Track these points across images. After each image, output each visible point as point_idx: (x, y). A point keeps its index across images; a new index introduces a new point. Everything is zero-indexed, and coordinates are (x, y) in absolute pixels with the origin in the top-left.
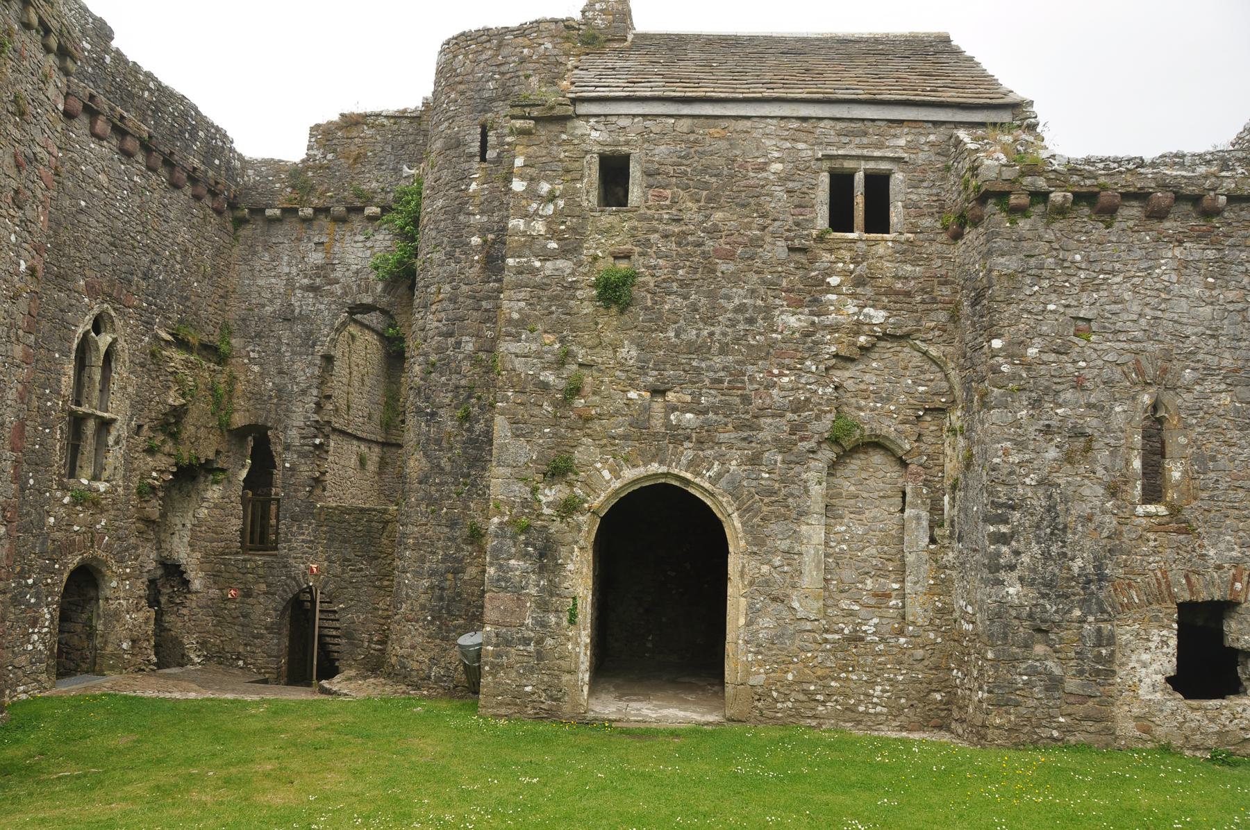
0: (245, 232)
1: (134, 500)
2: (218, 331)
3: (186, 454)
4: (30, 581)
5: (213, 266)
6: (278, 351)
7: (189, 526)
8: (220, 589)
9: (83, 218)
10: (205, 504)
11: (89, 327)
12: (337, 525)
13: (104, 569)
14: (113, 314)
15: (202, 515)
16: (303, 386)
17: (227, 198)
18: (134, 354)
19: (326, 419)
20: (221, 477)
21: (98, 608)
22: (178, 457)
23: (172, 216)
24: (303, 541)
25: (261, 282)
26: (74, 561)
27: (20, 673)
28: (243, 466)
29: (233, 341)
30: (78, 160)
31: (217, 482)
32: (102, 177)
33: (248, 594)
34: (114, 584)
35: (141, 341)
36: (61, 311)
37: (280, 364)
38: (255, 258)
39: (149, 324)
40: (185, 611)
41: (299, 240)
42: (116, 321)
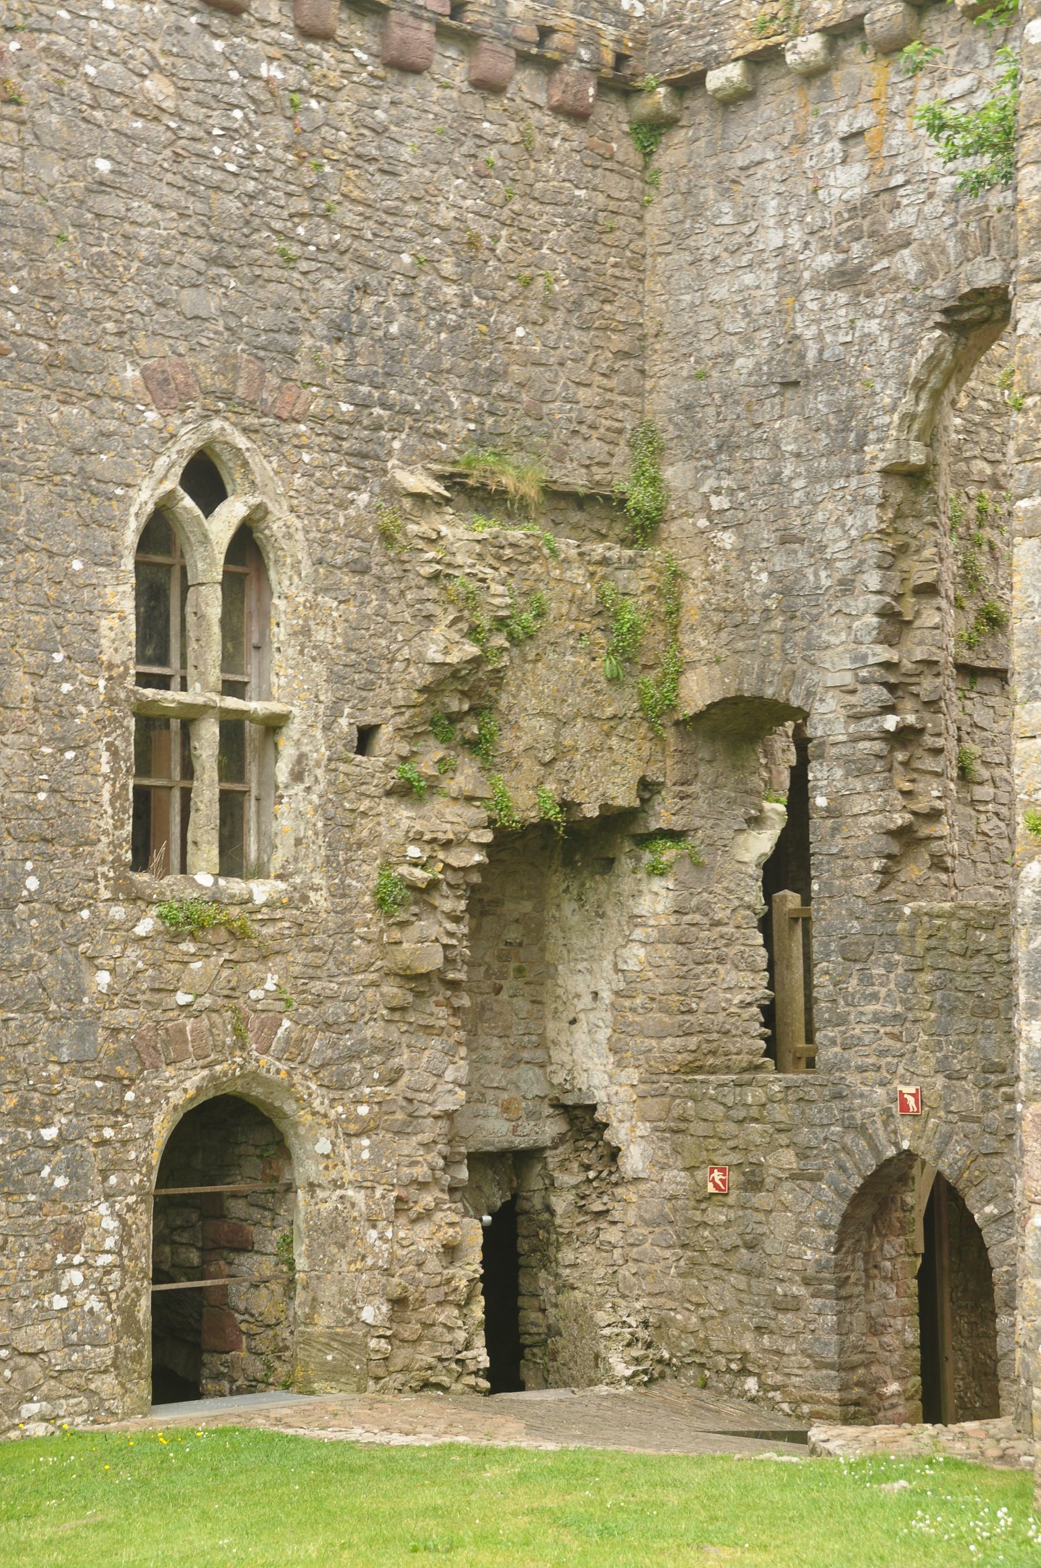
0: (672, 153)
1: (368, 921)
2: (622, 451)
3: (528, 800)
4: (49, 1134)
5: (579, 275)
6: (776, 478)
7: (606, 996)
8: (690, 1169)
9: (111, 204)
10: (639, 934)
11: (172, 483)
12: (960, 963)
13: (290, 1107)
14: (242, 442)
15: (633, 965)
16: (843, 567)
17: (595, 68)
19: (919, 654)
20: (669, 853)
21: (293, 1208)
22: (501, 802)
23: (406, 153)
24: (876, 1018)
25: (719, 291)
26: (184, 1086)
27: (34, 1367)
28: (756, 821)
29: (669, 473)
30: (71, 50)
31: (657, 871)
32: (156, 87)
33: (753, 1183)
34: (323, 1146)
35: (344, 505)
36: (78, 451)
37: (783, 514)
38: (701, 225)
39: (367, 460)
40: (612, 1235)
41: (801, 140)
42: (256, 461)
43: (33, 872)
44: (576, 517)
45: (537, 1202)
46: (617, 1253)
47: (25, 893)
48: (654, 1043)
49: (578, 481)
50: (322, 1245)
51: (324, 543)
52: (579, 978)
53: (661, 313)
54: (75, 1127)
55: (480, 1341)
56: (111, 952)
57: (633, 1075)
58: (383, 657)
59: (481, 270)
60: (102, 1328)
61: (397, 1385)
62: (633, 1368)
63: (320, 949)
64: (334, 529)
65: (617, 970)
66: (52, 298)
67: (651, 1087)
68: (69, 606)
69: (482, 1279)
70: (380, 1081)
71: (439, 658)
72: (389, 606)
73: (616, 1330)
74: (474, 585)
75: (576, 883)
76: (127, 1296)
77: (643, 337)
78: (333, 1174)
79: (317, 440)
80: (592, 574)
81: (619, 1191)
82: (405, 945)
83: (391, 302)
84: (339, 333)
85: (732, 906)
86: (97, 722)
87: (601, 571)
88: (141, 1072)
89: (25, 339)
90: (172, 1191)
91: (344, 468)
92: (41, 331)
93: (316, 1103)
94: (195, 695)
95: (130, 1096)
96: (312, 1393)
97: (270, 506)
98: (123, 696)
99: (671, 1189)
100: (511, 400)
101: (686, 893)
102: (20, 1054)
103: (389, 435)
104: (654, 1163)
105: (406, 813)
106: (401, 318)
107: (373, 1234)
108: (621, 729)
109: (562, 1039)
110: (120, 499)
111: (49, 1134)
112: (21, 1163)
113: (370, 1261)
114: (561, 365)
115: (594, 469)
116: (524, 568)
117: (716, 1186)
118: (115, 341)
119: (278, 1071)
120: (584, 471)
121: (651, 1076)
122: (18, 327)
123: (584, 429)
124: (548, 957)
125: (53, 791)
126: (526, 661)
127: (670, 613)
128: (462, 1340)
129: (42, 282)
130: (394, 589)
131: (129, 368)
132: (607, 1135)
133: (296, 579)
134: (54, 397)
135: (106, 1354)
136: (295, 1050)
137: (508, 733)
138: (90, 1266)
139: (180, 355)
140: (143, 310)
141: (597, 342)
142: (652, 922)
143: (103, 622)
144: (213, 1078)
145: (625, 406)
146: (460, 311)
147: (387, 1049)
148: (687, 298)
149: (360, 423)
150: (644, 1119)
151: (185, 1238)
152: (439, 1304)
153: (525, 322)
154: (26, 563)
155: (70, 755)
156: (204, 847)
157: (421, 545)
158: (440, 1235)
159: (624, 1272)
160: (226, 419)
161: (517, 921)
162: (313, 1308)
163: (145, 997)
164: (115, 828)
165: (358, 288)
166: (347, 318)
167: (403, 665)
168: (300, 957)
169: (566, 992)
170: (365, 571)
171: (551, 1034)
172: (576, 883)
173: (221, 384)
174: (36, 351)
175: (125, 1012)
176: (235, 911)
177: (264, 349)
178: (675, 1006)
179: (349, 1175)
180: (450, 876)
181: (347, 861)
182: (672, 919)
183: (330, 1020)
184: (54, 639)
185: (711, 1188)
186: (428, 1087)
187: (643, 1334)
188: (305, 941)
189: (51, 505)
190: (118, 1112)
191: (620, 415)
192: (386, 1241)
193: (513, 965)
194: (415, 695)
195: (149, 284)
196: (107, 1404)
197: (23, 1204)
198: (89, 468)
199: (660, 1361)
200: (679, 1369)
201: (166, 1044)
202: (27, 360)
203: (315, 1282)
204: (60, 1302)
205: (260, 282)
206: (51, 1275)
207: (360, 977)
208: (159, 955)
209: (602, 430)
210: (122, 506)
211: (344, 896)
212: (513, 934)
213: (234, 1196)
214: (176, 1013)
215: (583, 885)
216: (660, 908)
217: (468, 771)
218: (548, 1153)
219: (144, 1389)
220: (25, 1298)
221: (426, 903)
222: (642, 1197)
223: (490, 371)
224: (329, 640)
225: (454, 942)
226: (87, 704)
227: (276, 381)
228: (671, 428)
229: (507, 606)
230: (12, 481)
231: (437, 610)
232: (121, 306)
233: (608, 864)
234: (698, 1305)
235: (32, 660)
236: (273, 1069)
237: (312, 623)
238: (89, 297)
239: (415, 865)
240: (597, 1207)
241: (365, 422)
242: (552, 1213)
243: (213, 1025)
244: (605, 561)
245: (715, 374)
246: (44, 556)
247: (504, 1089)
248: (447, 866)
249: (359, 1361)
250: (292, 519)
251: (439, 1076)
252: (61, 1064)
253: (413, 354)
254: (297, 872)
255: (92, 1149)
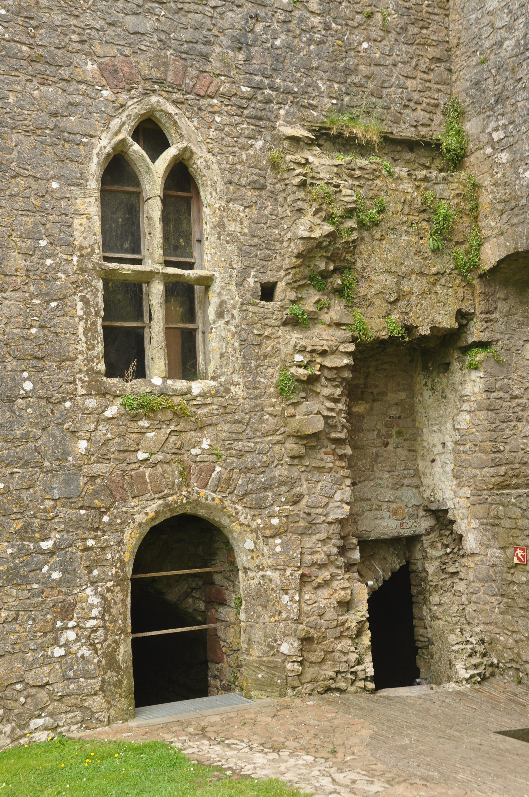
1: (273, 404)
2: (438, 117)
3: (379, 324)
4: (47, 545)
7: (450, 445)
8: (503, 548)
10: (466, 406)
13: (225, 521)
14: (172, 109)
15: (463, 426)
18: (233, 172)
20: (480, 356)
26: (146, 511)
27: (43, 695)
36: (54, 115)
39: (262, 122)
40: (461, 586)
43: (28, 379)
44: (408, 156)
45: (419, 566)
46: (464, 597)
47: (22, 392)
48: (478, 471)
49: (410, 133)
50: (252, 606)
51: (233, 172)
52: (435, 435)
53: (459, 32)
54: (66, 540)
55: (368, 659)
56: (87, 428)
57: (467, 491)
58: (277, 240)
59: (337, 8)
60: (91, 667)
61: (308, 691)
62: (471, 672)
63: (240, 422)
64: (239, 163)
65: (455, 429)
66: (32, 18)
67: (478, 499)
68: (50, 211)
69: (368, 619)
70: (286, 503)
71: (306, 234)
72: (279, 208)
73: (462, 647)
74: (331, 189)
75: (430, 380)
76: (109, 645)
77: (449, 50)
78: (257, 562)
79: (226, 109)
80: (418, 187)
81: (464, 560)
82: (298, 417)
83: (275, 26)
84: (239, 45)
85: (524, 387)
86: (73, 283)
87: (423, 185)
88: (113, 503)
89: (12, 44)
90: (138, 576)
91: (245, 126)
92: (24, 39)
93: (242, 518)
94: (147, 266)
95: (106, 519)
96: (250, 698)
97: (194, 149)
98: (90, 266)
99: (493, 560)
100: (361, 86)
101: (492, 379)
102: (24, 495)
103: (277, 107)
104: (482, 544)
105: (296, 336)
106: (283, 36)
107: (286, 598)
108: (443, 281)
109: (427, 471)
110: (86, 145)
111: (47, 545)
112: (26, 564)
113: (284, 615)
114: (395, 65)
115: (420, 128)
116: (370, 182)
117: (519, 559)
118: (78, 46)
119: (213, 499)
120: (413, 129)
121: (477, 492)
122: (7, 36)
123: (412, 104)
124: (417, 424)
125: (42, 327)
126: (373, 239)
127: (471, 210)
128: (353, 660)
129: (23, 8)
130: (281, 198)
131: (89, 63)
132: (455, 527)
133: (214, 194)
134: (35, 81)
135: (95, 683)
136: (225, 485)
137: (363, 283)
138: (82, 628)
139: (126, 56)
140: (98, 27)
141: (418, 52)
142: (473, 398)
143: (76, 221)
144: (167, 505)
145: (439, 90)
146: (323, 32)
147: (293, 483)
148: (474, 16)
149: (256, 98)
150: (475, 518)
151: (197, 594)
152: (336, 638)
153: (368, 39)
154: (17, 184)
155: (54, 304)
156: (157, 361)
157: (293, 166)
158: (336, 595)
159: (470, 609)
160: (160, 95)
161: (396, 404)
162: (249, 644)
163: (113, 456)
164: (88, 349)
165: (251, 17)
166: (245, 36)
167: (287, 243)
168: (226, 427)
169: (428, 444)
170: (263, 188)
171: (421, 469)
172: (430, 380)
173: (156, 74)
174: (20, 51)
175: (99, 465)
176: (177, 400)
177: (186, 53)
178: (488, 449)
179: (267, 562)
180: (326, 373)
181: (257, 367)
182: (484, 396)
183: (249, 466)
184: (40, 232)
185: (516, 561)
186: (323, 505)
187: (480, 649)
188: (229, 417)
189: (35, 148)
190: (98, 529)
191: (436, 96)
192: (295, 602)
193: (395, 430)
194: (294, 260)
195: (102, 11)
196: (97, 715)
197: (29, 591)
198: (62, 125)
199: (492, 665)
200: (504, 670)
201: (131, 485)
202: (14, 57)
203: (249, 629)
204: (59, 652)
205: (183, 13)
206: (53, 635)
207: (269, 438)
208: (123, 429)
209: (424, 105)
210: (87, 149)
211: (255, 388)
212: (394, 412)
213: (216, 572)
214: (137, 465)
215: (434, 380)
216: (477, 390)
217: (337, 308)
218: (424, 538)
219: (125, 703)
220: (34, 650)
221: (311, 390)
222: (476, 564)
223: (346, 68)
224: (238, 229)
225: (333, 414)
226: (65, 272)
227: (195, 73)
228: (468, 99)
229: (354, 202)
230: (5, 133)
231: (306, 206)
232: (82, 25)
233: (446, 367)
234: (513, 632)
235: (23, 245)
236: (210, 498)
237: (225, 220)
238: (57, 18)
239: (300, 366)
240: (452, 570)
241: (259, 98)
242: (427, 573)
243: (165, 472)
244: (426, 179)
245: (492, 57)
246: (31, 180)
247: (393, 502)
248: (323, 367)
249: (280, 677)
250: (210, 156)
251: (331, 497)
252: (55, 500)
253: (291, 58)
254: (222, 374)
255: (80, 553)
